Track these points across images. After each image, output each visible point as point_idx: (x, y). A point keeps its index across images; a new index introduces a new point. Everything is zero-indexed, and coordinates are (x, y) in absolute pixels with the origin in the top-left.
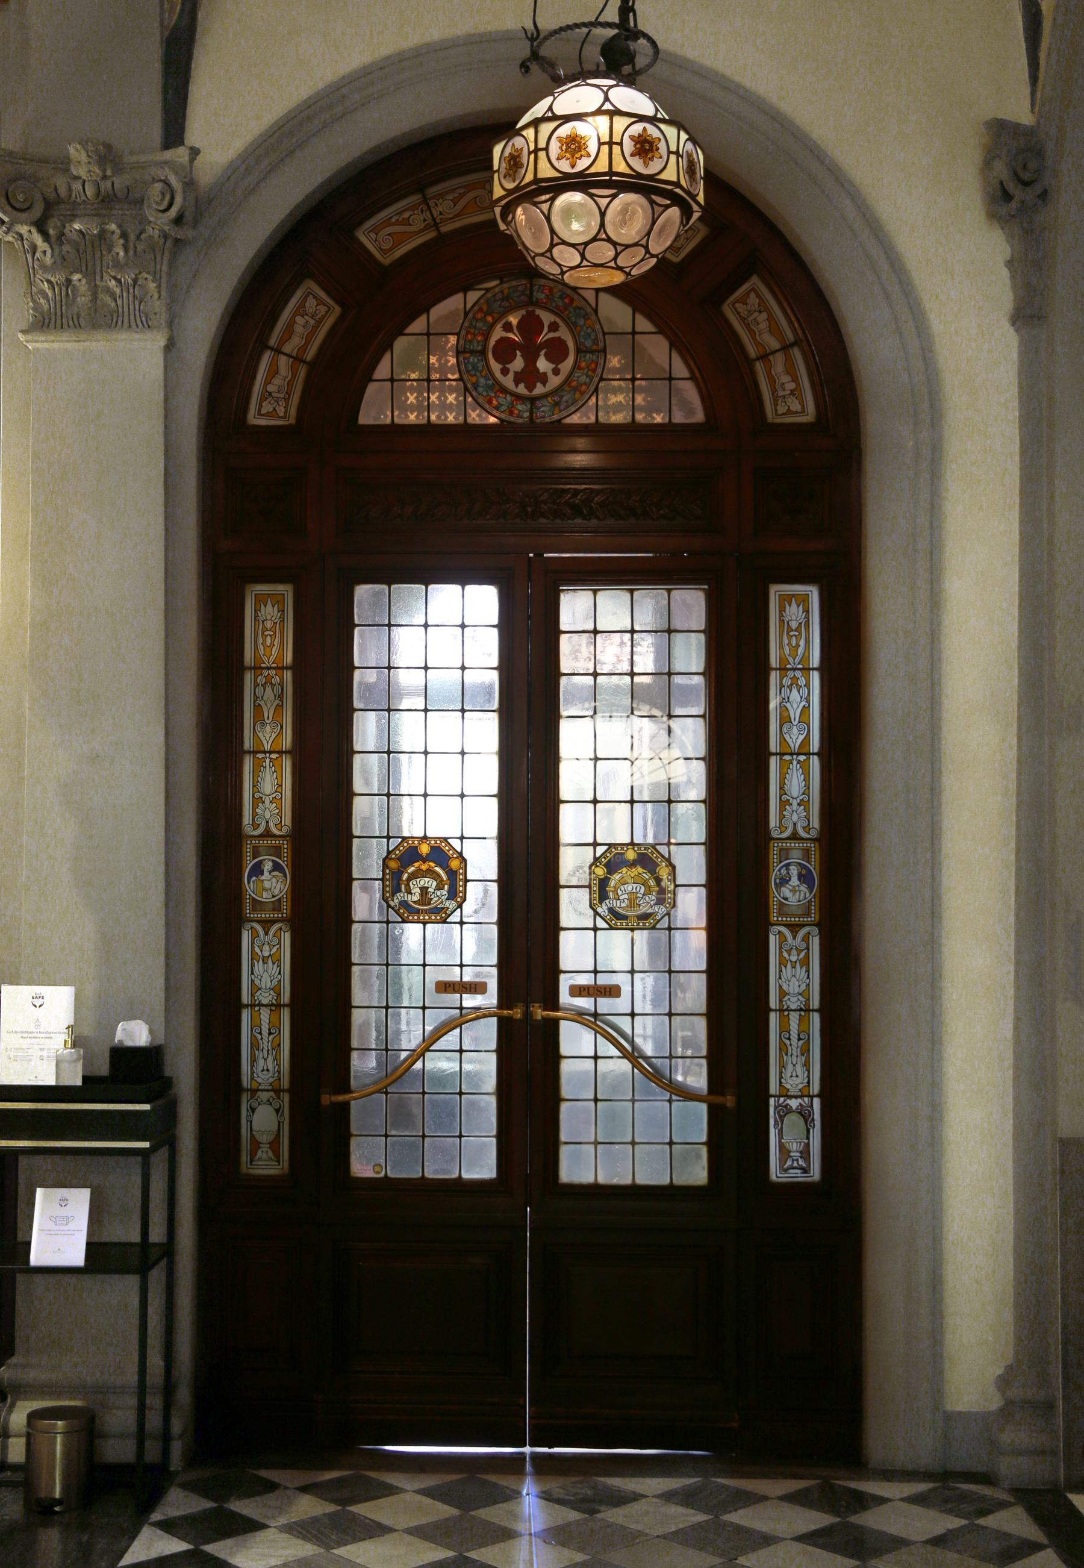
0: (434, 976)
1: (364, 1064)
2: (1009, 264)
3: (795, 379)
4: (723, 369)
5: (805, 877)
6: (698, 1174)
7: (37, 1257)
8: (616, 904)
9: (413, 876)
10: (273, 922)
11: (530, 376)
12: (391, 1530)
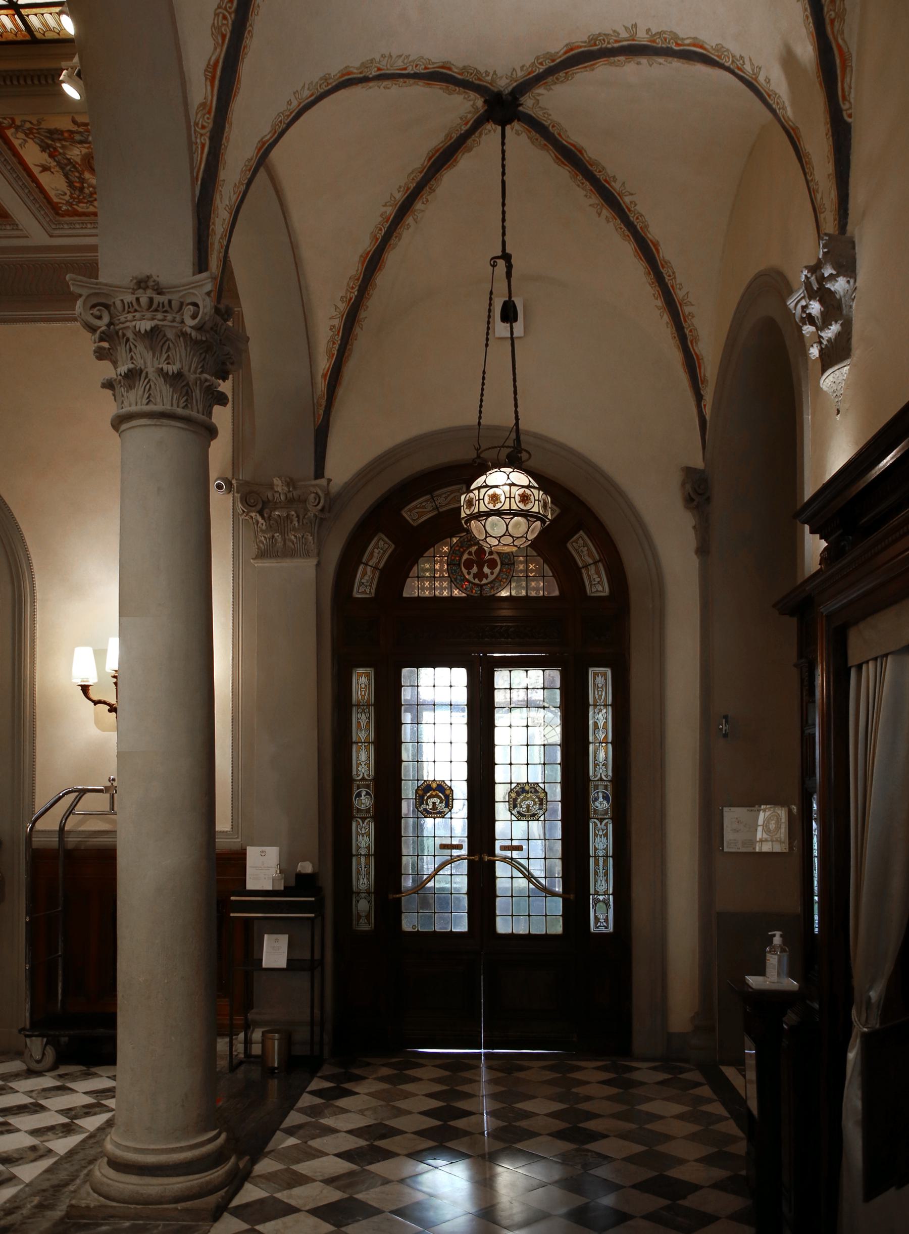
0: (439, 842)
1: (408, 883)
2: (694, 527)
3: (600, 577)
4: (567, 572)
5: (606, 798)
6: (557, 928)
7: (265, 965)
8: (521, 809)
9: (429, 797)
10: (366, 818)
11: (480, 575)
12: (421, 1079)
